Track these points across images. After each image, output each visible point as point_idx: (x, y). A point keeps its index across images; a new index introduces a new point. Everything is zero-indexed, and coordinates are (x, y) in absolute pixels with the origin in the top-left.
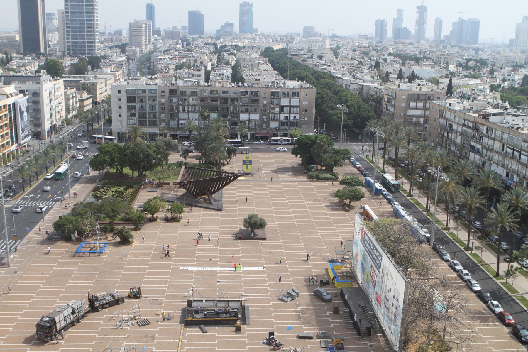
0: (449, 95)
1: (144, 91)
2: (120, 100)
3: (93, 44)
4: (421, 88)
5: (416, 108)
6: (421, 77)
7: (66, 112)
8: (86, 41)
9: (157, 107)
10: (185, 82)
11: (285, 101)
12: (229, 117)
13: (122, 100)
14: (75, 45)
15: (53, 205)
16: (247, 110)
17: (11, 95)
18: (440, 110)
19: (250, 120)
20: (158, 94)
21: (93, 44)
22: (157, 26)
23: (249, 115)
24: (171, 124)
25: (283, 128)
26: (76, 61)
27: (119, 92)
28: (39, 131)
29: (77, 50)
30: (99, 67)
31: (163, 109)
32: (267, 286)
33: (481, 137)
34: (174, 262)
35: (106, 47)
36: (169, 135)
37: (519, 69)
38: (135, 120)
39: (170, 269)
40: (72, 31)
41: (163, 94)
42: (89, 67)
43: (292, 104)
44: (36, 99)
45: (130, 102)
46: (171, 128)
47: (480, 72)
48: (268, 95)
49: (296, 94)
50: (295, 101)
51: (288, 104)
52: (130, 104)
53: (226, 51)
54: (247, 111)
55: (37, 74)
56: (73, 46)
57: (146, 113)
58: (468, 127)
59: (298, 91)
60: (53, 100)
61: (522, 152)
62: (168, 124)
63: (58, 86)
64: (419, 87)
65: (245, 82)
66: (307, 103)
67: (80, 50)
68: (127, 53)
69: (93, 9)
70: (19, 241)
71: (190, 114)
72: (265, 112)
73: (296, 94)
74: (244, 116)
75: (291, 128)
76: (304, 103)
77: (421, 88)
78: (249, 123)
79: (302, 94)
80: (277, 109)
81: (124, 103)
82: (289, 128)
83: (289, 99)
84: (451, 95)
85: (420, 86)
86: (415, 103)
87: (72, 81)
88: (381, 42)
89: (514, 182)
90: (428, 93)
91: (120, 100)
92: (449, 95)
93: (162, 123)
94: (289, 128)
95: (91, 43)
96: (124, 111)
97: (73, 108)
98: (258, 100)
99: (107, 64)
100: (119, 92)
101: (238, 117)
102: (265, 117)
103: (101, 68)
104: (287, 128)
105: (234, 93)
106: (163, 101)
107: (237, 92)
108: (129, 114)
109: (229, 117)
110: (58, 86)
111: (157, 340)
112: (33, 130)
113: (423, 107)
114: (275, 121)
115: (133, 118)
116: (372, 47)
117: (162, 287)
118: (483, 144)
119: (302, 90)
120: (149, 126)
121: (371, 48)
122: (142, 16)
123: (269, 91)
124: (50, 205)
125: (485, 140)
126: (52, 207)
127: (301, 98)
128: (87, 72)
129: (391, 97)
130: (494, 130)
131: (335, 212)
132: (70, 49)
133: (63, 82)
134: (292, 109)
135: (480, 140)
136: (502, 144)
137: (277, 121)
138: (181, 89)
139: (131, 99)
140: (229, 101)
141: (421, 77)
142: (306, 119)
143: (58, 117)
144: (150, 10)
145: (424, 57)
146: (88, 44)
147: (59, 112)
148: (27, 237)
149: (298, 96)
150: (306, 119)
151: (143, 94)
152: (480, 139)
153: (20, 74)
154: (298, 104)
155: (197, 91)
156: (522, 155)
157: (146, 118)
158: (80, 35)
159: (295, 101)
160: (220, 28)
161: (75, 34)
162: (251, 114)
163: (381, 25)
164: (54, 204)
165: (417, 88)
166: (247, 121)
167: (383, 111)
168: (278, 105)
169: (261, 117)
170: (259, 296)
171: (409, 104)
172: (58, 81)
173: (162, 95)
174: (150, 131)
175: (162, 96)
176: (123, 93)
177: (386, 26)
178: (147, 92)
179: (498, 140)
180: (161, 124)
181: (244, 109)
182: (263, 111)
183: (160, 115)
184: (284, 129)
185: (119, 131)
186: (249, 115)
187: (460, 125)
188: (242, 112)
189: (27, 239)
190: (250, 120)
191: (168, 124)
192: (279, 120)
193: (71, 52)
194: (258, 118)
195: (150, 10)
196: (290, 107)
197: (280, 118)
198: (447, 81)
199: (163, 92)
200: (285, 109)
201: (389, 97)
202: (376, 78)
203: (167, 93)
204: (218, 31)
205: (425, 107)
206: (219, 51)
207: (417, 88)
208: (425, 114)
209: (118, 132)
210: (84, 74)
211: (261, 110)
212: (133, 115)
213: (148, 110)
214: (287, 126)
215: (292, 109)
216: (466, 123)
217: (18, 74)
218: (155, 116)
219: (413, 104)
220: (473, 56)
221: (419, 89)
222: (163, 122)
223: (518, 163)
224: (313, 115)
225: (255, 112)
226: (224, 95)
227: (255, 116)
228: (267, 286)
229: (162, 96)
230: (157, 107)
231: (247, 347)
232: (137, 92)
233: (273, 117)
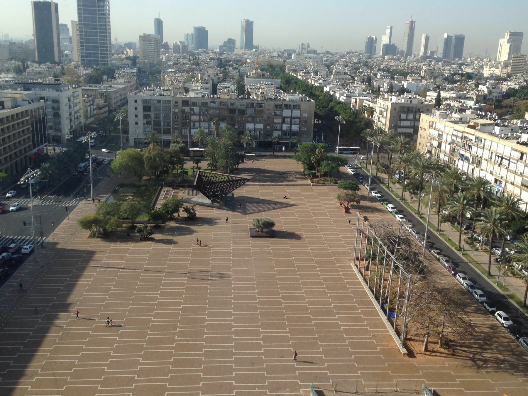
0: (437, 107)
1: (159, 101)
2: (136, 109)
3: (106, 56)
4: (411, 101)
5: (407, 120)
6: (411, 91)
7: (84, 119)
8: (99, 52)
9: (171, 115)
10: (197, 94)
11: (287, 113)
12: (236, 127)
13: (138, 109)
14: (89, 55)
15: (76, 205)
16: (253, 120)
17: (32, 100)
18: (430, 121)
19: (255, 130)
20: (172, 103)
21: (106, 56)
22: (165, 40)
23: (255, 125)
24: (183, 132)
25: (285, 137)
26: (89, 71)
27: (136, 101)
28: (59, 136)
29: (91, 60)
30: (114, 78)
31: (176, 118)
32: (276, 279)
33: (470, 146)
34: (191, 257)
35: (395, 298)
36: (181, 142)
37: (503, 82)
38: (149, 128)
39: (189, 264)
40: (86, 42)
41: (176, 104)
42: (105, 77)
43: (293, 116)
44: (55, 105)
45: (146, 111)
46: (184, 135)
47: (466, 86)
48: (272, 107)
49: (297, 107)
50: (296, 113)
51: (290, 116)
52: (146, 113)
53: (230, 66)
54: (253, 121)
55: (56, 81)
56: (87, 57)
57: (160, 122)
58: (457, 136)
59: (299, 103)
60: (72, 106)
61: (511, 160)
62: (181, 132)
63: (77, 93)
64: (410, 100)
65: (251, 95)
66: (306, 115)
67: (94, 61)
68: (138, 65)
69: (106, 22)
70: (45, 238)
71: (201, 123)
72: (268, 122)
73: (297, 107)
74: (250, 126)
75: (292, 137)
76: (304, 115)
77: (411, 101)
78: (254, 133)
79: (303, 106)
80: (280, 120)
81: (140, 111)
82: (290, 138)
83: (290, 111)
84: (439, 107)
85: (411, 99)
86: (406, 115)
87: (88, 89)
88: (370, 58)
89: (502, 188)
90: (418, 106)
91: (136, 109)
92: (437, 107)
93: (176, 131)
94: (290, 138)
95: (104, 54)
96: (141, 120)
97: (91, 114)
98: (262, 111)
99: (120, 75)
100: (136, 101)
101: (244, 127)
102: (268, 127)
103: (114, 78)
104: (289, 137)
105: (241, 105)
106: (176, 111)
107: (244, 103)
108: (145, 122)
109: (236, 127)
110: (77, 93)
111: (179, 329)
112: (53, 134)
113: (413, 118)
114: (278, 130)
115: (148, 125)
116: (363, 63)
117: (182, 280)
118: (472, 152)
119: (302, 102)
120: (164, 133)
121: (362, 64)
122: (151, 30)
123: (272, 103)
124: (73, 205)
125: (474, 149)
126: (75, 207)
127: (302, 110)
128: (103, 81)
129: (383, 110)
130: (483, 140)
131: (105, 243)
132: (84, 59)
133: (81, 91)
134: (293, 120)
135: (469, 149)
136: (491, 152)
137: (279, 130)
138: (192, 101)
139: (147, 108)
140: (237, 112)
141: (411, 91)
142: (305, 129)
143: (77, 123)
144: (159, 23)
145: (411, 71)
146: (101, 55)
147: (77, 118)
148: (52, 234)
149: (299, 109)
150: (305, 129)
151: (158, 104)
152: (470, 147)
153: (37, 81)
154: (298, 115)
155: (207, 103)
156: (511, 163)
157: (160, 126)
158: (93, 46)
159: (296, 113)
160: (222, 44)
161: (89, 46)
162: (256, 124)
163: (371, 43)
164: (78, 204)
165: (408, 101)
166: (253, 130)
167: (375, 123)
168: (281, 116)
169: (265, 127)
170: (270, 288)
171: (400, 116)
172: (77, 90)
173: (175, 106)
174: (165, 139)
175: (176, 106)
176: (140, 102)
177: (376, 43)
178: (162, 102)
179: (487, 149)
180: (174, 132)
181: (249, 119)
182: (267, 122)
183: (173, 123)
184: (285, 138)
185: (136, 138)
186: (255, 125)
187: (449, 135)
188: (248, 122)
189: (53, 236)
190: (255, 130)
191: (181, 132)
192: (281, 130)
193: (85, 62)
194: (262, 128)
195: (159, 23)
196: (292, 118)
197: (282, 128)
198: (435, 94)
199: (176, 102)
200: (286, 120)
201: (381, 109)
202: (368, 91)
203: (180, 103)
204: (221, 47)
205: (415, 119)
206: (222, 64)
207: (408, 101)
208: (414, 125)
209: (135, 139)
210: (100, 84)
211: (266, 120)
212: (148, 123)
213: (162, 119)
214: (288, 135)
215: (293, 120)
216: (455, 133)
217: (35, 81)
218: (168, 124)
219: (403, 116)
220: (458, 71)
221: (409, 102)
222: (177, 130)
223: (506, 170)
224: (312, 125)
225: (260, 122)
226: (232, 107)
227: (260, 126)
228: (276, 279)
229: (176, 106)
230: (171, 115)
231: (261, 335)
232: (152, 102)
233: (276, 127)
